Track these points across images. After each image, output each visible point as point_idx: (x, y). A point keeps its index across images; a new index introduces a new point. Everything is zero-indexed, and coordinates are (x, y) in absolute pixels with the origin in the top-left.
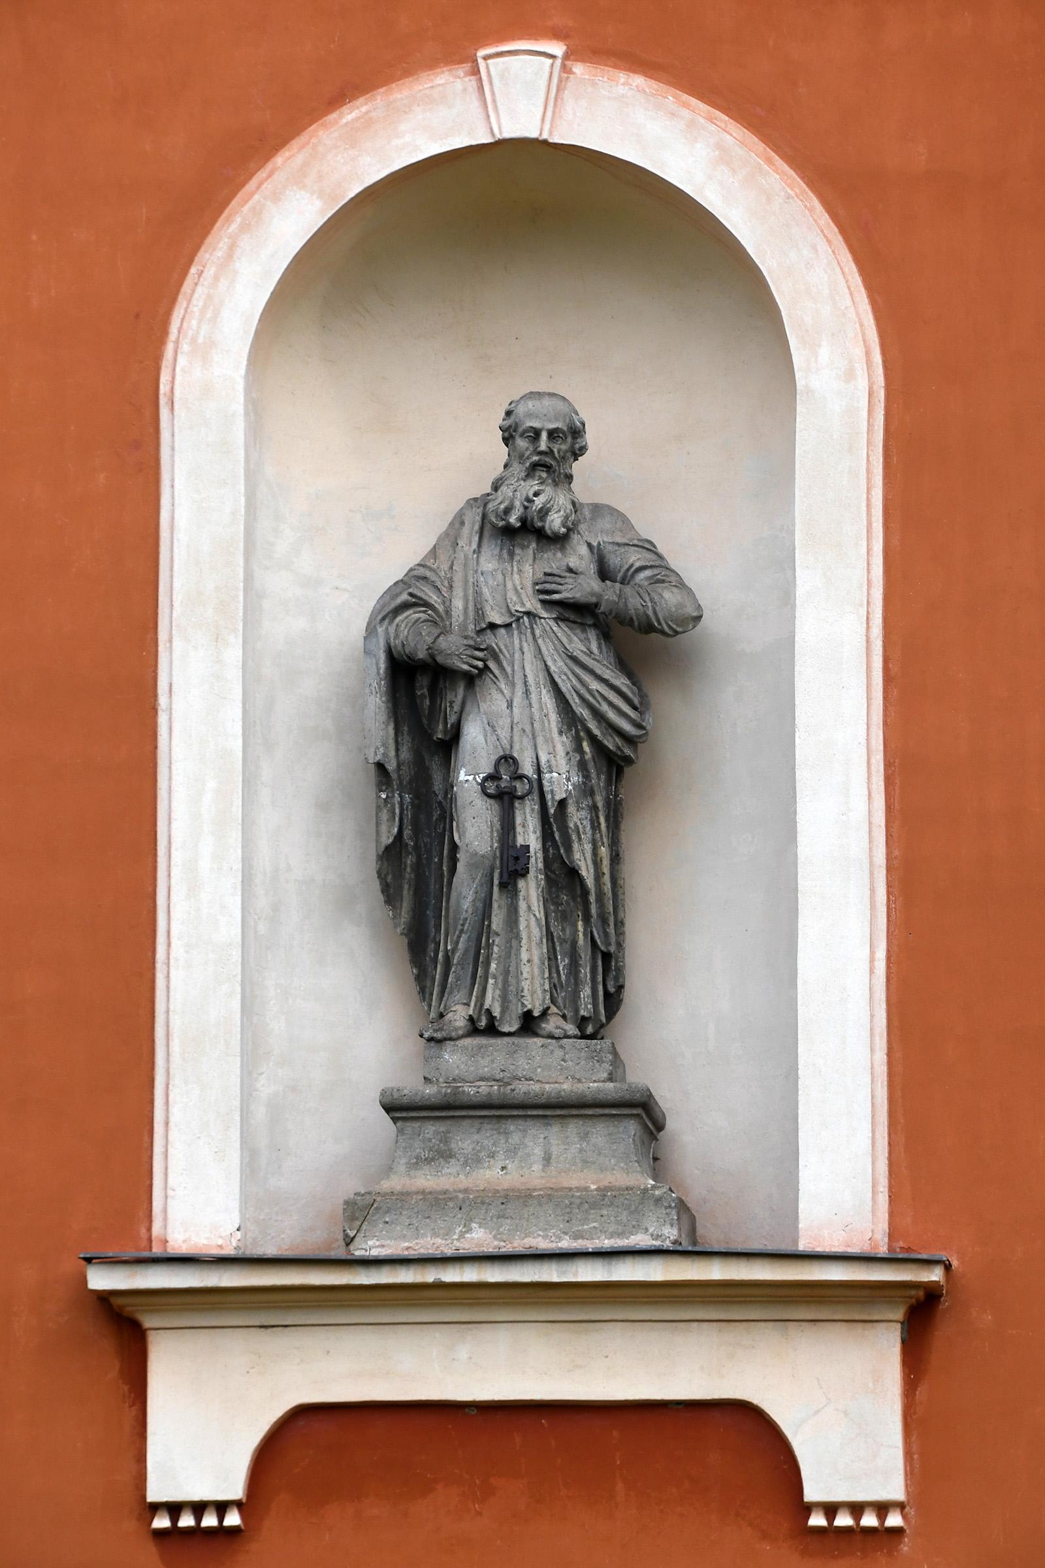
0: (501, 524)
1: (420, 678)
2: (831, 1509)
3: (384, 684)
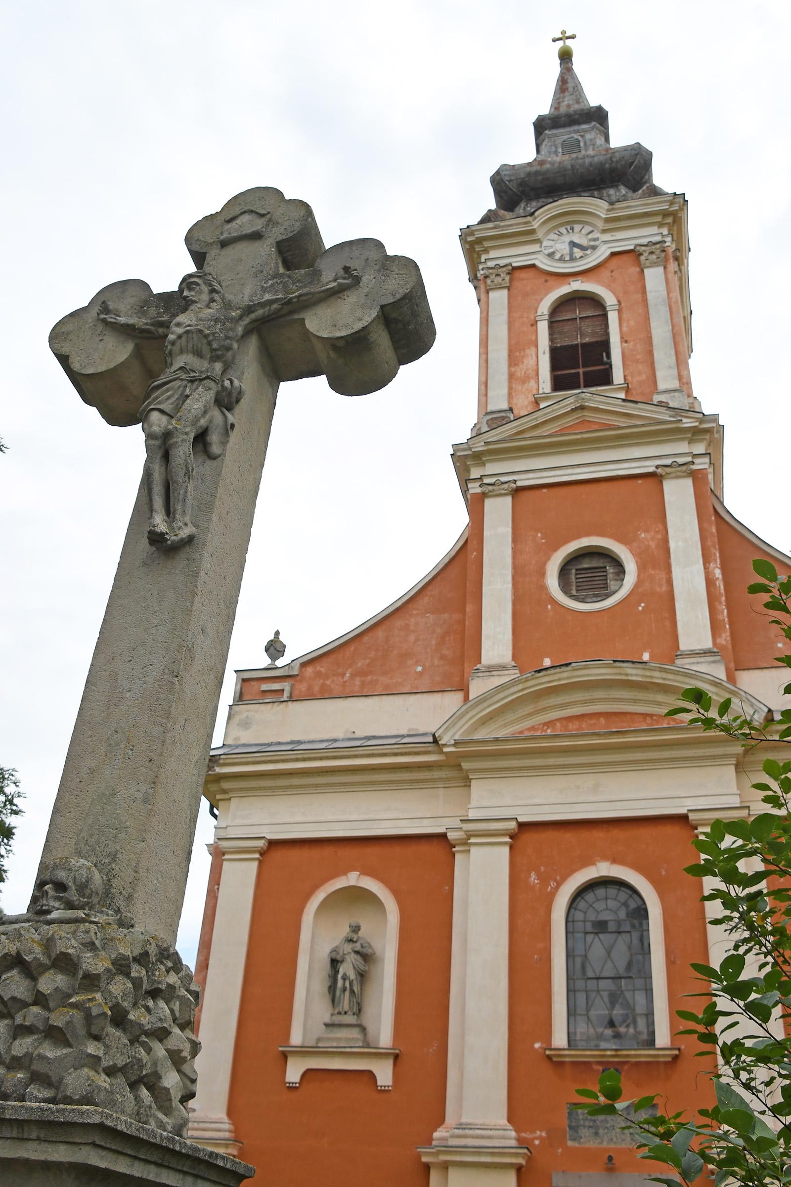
2: (381, 1087)
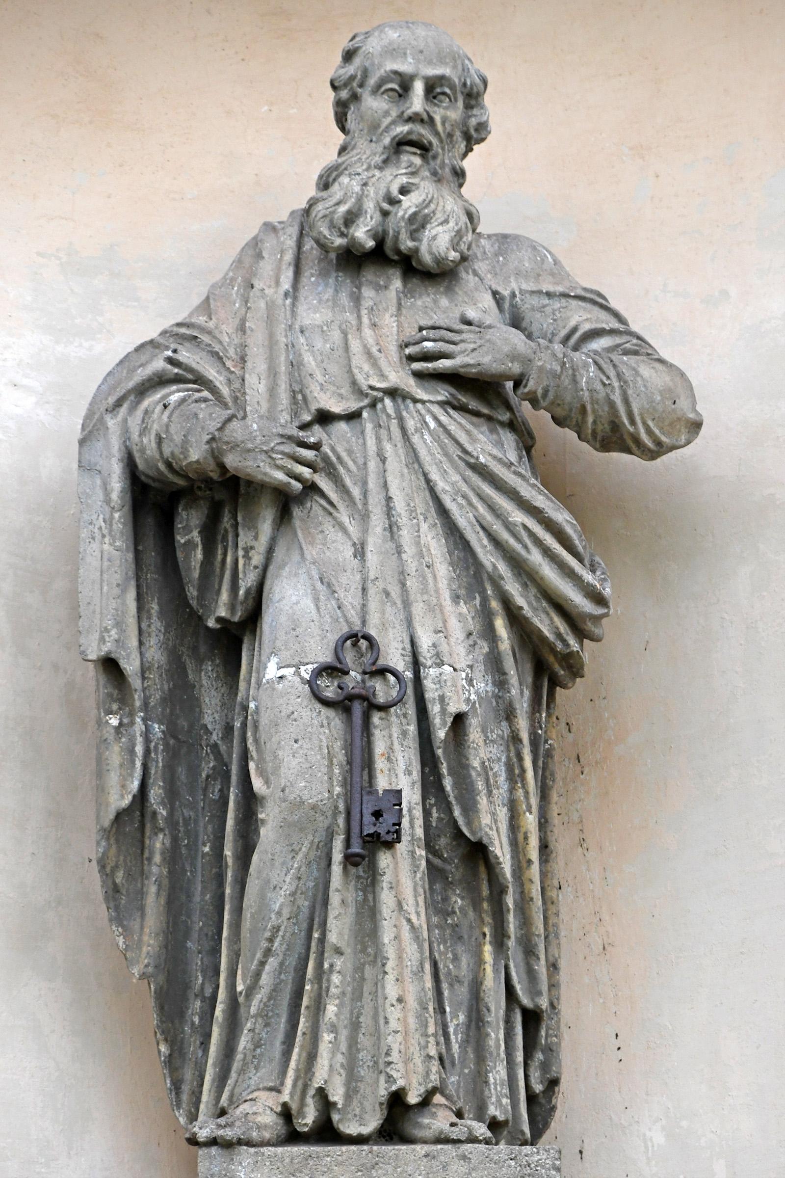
0: (339, 241)
1: (184, 514)
3: (120, 517)
